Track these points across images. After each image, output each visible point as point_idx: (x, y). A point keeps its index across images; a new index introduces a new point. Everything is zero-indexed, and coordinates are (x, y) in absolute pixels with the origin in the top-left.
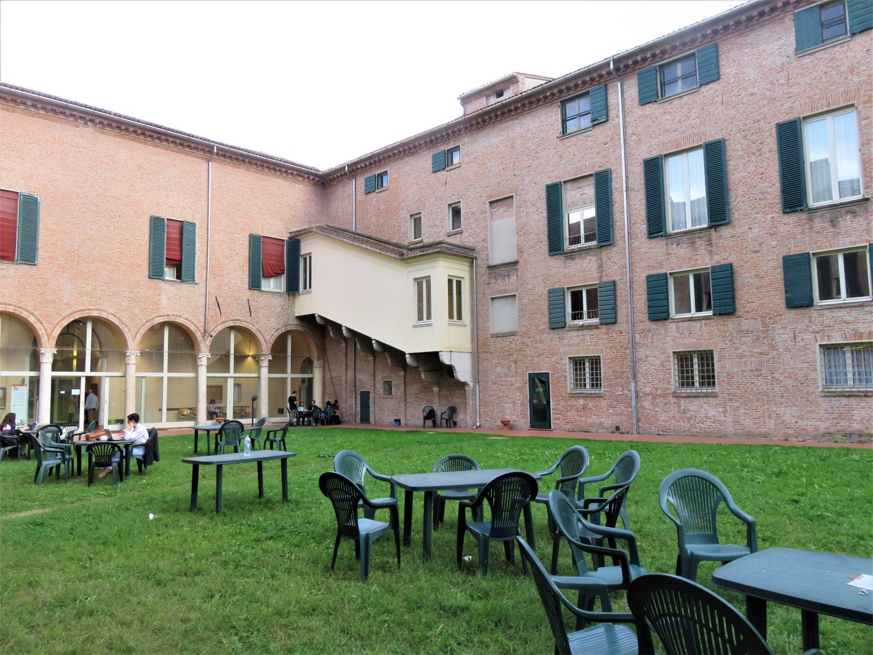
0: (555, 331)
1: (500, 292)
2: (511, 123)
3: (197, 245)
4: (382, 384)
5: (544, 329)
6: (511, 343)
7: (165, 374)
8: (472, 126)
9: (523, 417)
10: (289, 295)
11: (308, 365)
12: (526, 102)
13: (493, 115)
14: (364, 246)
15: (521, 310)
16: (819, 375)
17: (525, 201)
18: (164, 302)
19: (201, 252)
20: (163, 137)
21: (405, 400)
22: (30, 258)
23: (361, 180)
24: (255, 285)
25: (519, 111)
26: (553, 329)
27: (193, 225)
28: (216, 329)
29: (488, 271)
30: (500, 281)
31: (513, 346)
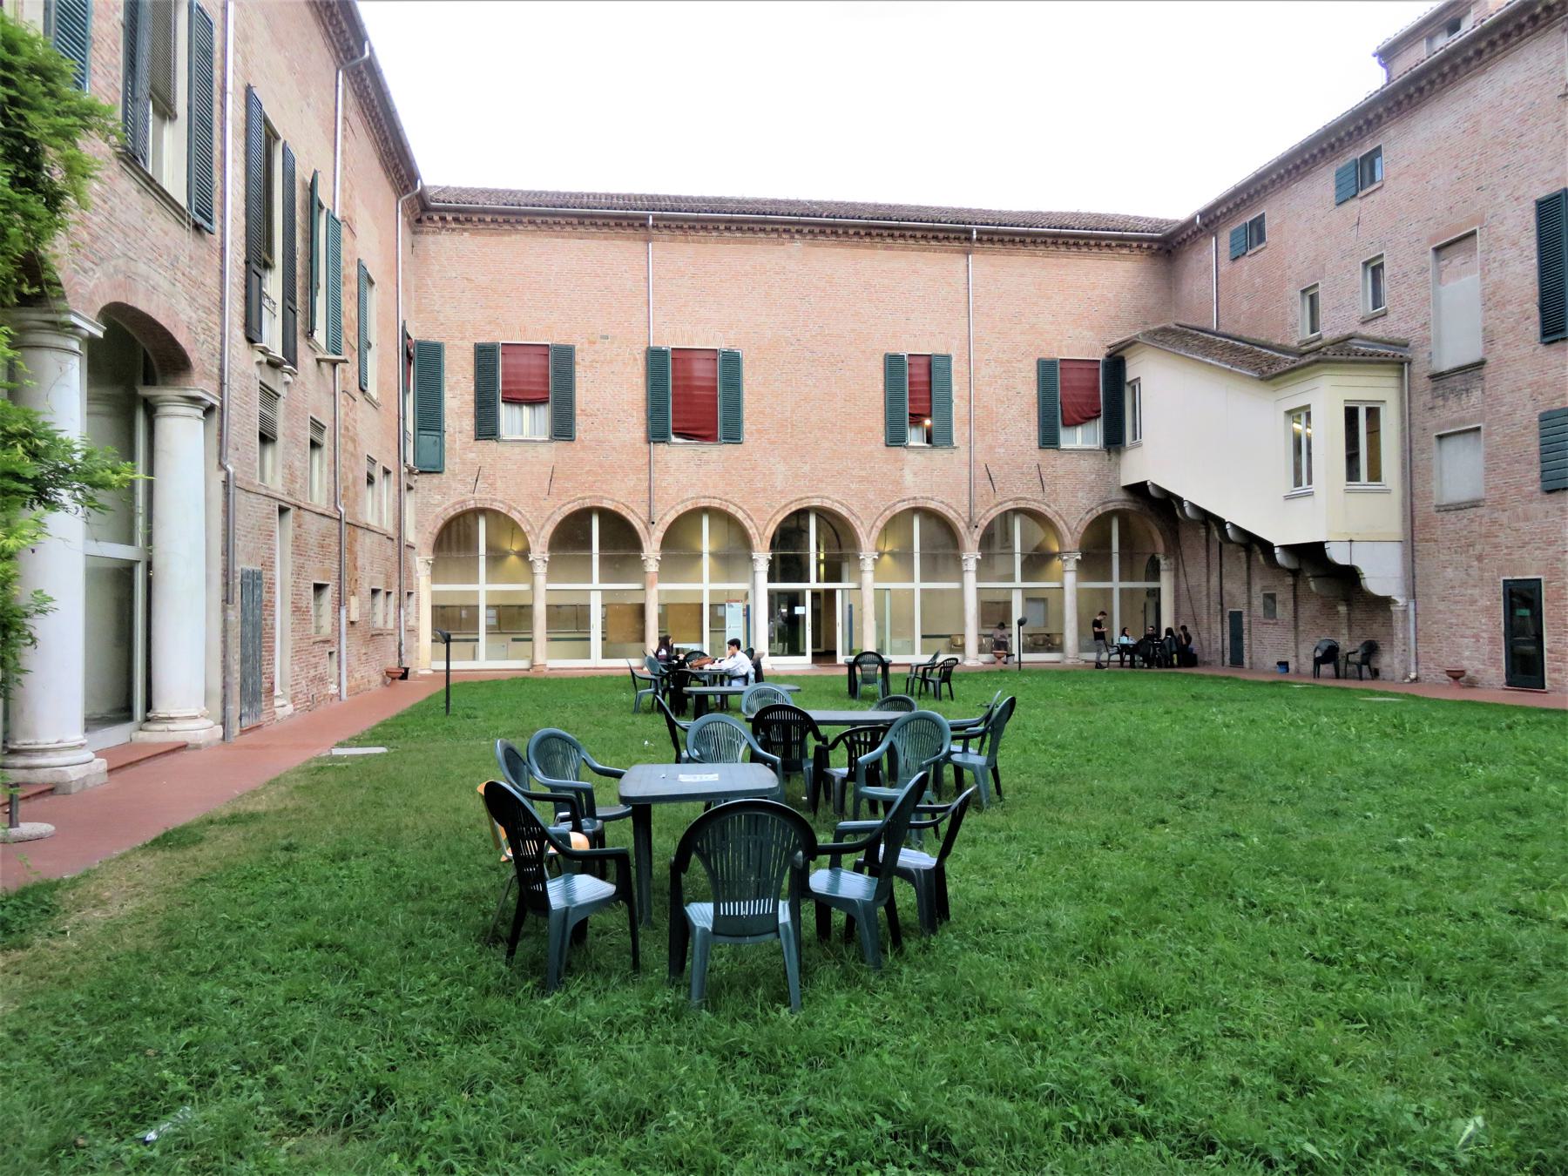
0: (1553, 496)
1: (1453, 423)
2: (1471, 83)
3: (955, 388)
4: (1261, 600)
5: (1532, 493)
6: (1472, 521)
7: (917, 585)
8: (1399, 104)
9: (1493, 665)
10: (1109, 451)
11: (1154, 572)
12: (1496, 36)
13: (1434, 75)
14: (1208, 360)
15: (1490, 457)
17: (1498, 239)
18: (909, 478)
19: (961, 397)
20: (897, 233)
21: (1296, 627)
22: (734, 436)
23: (1225, 236)
24: (1049, 439)
25: (1485, 57)
26: (1549, 492)
27: (948, 358)
28: (987, 514)
29: (1431, 385)
30: (1453, 402)
31: (1475, 527)
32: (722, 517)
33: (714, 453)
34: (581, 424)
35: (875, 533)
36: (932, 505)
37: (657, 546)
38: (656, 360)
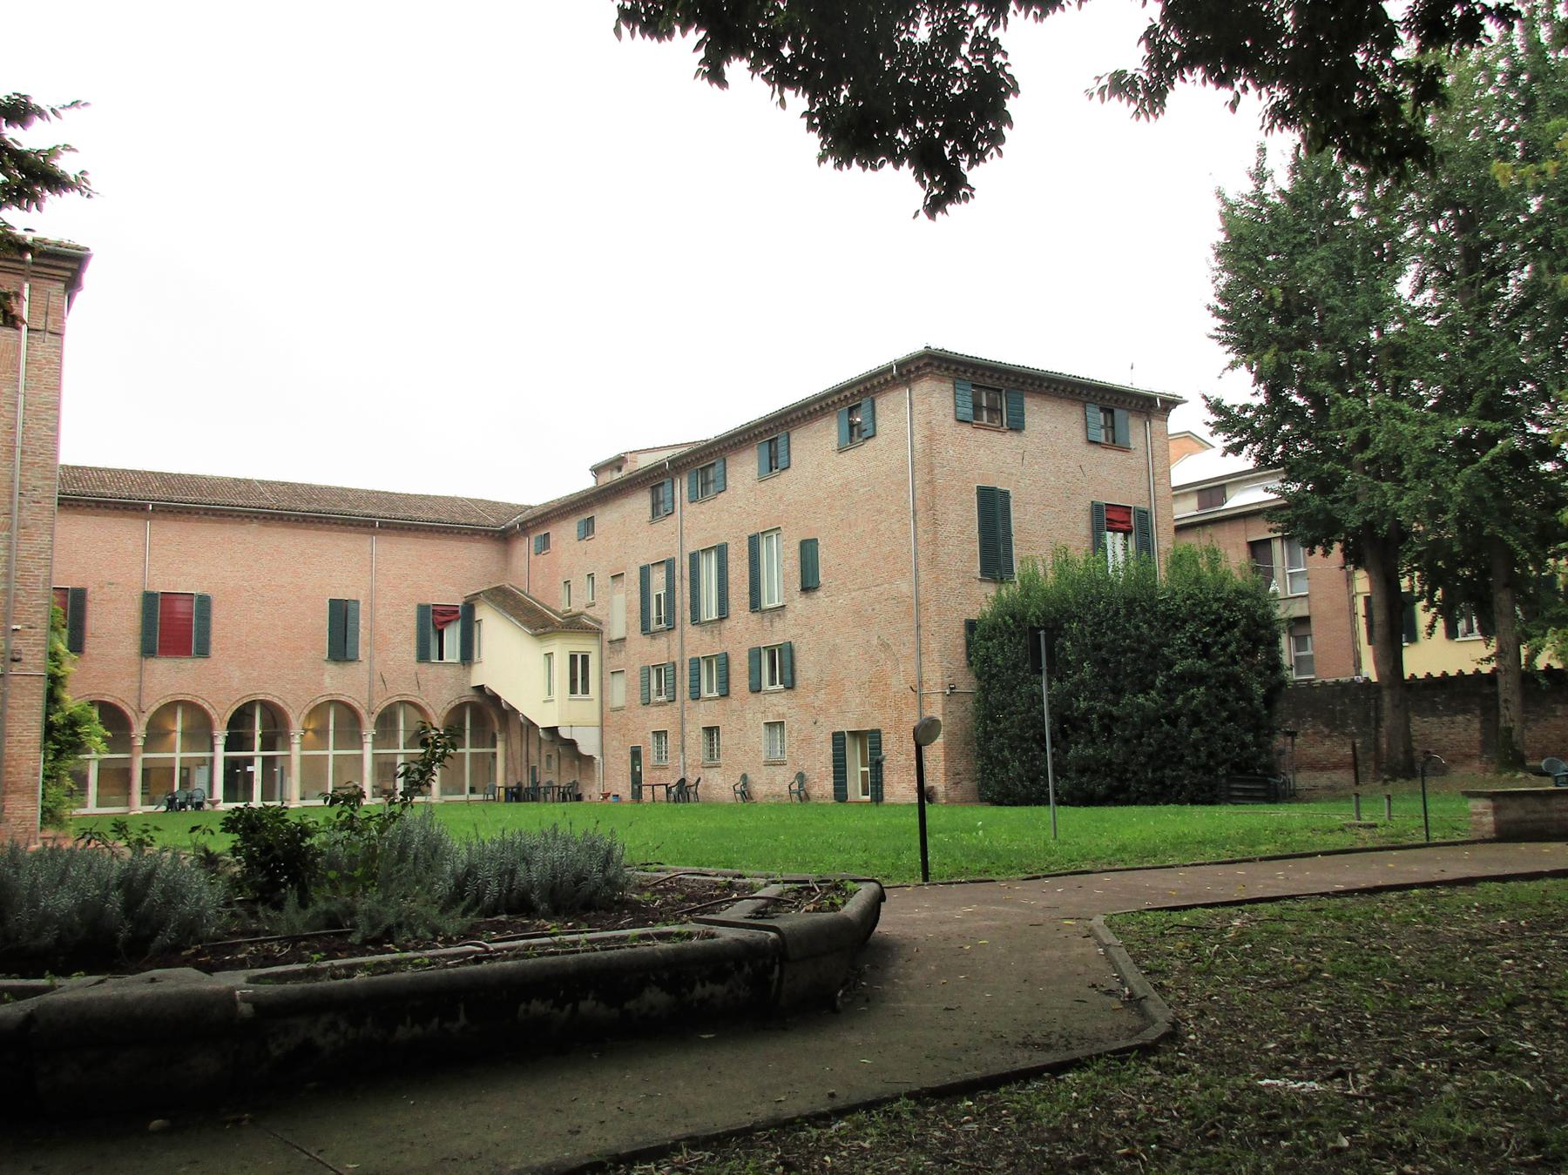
7: (331, 752)
16: (763, 747)
18: (327, 681)
22: (204, 652)
27: (357, 602)
28: (380, 705)
32: (191, 708)
33: (188, 664)
34: (90, 644)
35: (302, 717)
36: (342, 699)
37: (143, 728)
38: (149, 599)
